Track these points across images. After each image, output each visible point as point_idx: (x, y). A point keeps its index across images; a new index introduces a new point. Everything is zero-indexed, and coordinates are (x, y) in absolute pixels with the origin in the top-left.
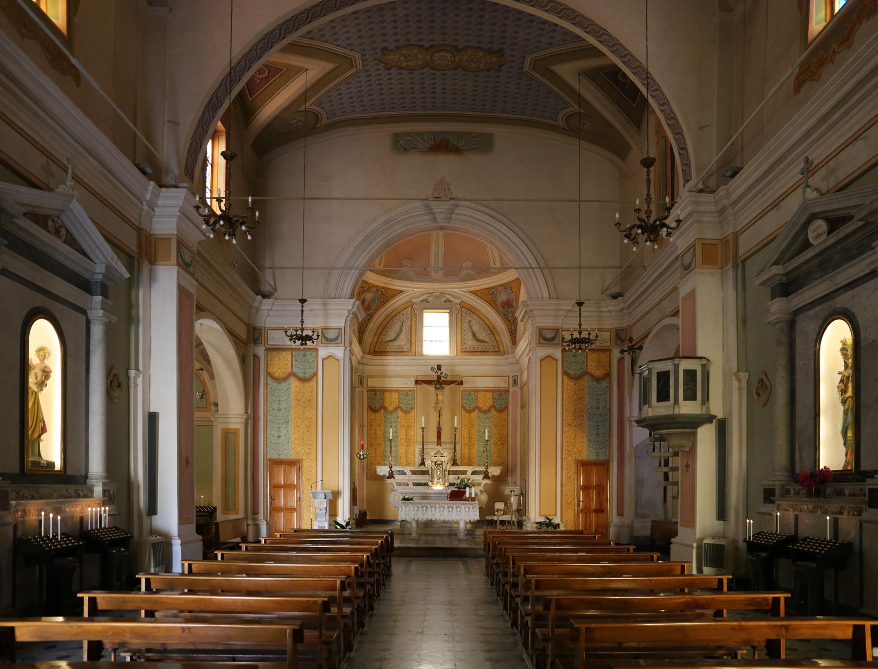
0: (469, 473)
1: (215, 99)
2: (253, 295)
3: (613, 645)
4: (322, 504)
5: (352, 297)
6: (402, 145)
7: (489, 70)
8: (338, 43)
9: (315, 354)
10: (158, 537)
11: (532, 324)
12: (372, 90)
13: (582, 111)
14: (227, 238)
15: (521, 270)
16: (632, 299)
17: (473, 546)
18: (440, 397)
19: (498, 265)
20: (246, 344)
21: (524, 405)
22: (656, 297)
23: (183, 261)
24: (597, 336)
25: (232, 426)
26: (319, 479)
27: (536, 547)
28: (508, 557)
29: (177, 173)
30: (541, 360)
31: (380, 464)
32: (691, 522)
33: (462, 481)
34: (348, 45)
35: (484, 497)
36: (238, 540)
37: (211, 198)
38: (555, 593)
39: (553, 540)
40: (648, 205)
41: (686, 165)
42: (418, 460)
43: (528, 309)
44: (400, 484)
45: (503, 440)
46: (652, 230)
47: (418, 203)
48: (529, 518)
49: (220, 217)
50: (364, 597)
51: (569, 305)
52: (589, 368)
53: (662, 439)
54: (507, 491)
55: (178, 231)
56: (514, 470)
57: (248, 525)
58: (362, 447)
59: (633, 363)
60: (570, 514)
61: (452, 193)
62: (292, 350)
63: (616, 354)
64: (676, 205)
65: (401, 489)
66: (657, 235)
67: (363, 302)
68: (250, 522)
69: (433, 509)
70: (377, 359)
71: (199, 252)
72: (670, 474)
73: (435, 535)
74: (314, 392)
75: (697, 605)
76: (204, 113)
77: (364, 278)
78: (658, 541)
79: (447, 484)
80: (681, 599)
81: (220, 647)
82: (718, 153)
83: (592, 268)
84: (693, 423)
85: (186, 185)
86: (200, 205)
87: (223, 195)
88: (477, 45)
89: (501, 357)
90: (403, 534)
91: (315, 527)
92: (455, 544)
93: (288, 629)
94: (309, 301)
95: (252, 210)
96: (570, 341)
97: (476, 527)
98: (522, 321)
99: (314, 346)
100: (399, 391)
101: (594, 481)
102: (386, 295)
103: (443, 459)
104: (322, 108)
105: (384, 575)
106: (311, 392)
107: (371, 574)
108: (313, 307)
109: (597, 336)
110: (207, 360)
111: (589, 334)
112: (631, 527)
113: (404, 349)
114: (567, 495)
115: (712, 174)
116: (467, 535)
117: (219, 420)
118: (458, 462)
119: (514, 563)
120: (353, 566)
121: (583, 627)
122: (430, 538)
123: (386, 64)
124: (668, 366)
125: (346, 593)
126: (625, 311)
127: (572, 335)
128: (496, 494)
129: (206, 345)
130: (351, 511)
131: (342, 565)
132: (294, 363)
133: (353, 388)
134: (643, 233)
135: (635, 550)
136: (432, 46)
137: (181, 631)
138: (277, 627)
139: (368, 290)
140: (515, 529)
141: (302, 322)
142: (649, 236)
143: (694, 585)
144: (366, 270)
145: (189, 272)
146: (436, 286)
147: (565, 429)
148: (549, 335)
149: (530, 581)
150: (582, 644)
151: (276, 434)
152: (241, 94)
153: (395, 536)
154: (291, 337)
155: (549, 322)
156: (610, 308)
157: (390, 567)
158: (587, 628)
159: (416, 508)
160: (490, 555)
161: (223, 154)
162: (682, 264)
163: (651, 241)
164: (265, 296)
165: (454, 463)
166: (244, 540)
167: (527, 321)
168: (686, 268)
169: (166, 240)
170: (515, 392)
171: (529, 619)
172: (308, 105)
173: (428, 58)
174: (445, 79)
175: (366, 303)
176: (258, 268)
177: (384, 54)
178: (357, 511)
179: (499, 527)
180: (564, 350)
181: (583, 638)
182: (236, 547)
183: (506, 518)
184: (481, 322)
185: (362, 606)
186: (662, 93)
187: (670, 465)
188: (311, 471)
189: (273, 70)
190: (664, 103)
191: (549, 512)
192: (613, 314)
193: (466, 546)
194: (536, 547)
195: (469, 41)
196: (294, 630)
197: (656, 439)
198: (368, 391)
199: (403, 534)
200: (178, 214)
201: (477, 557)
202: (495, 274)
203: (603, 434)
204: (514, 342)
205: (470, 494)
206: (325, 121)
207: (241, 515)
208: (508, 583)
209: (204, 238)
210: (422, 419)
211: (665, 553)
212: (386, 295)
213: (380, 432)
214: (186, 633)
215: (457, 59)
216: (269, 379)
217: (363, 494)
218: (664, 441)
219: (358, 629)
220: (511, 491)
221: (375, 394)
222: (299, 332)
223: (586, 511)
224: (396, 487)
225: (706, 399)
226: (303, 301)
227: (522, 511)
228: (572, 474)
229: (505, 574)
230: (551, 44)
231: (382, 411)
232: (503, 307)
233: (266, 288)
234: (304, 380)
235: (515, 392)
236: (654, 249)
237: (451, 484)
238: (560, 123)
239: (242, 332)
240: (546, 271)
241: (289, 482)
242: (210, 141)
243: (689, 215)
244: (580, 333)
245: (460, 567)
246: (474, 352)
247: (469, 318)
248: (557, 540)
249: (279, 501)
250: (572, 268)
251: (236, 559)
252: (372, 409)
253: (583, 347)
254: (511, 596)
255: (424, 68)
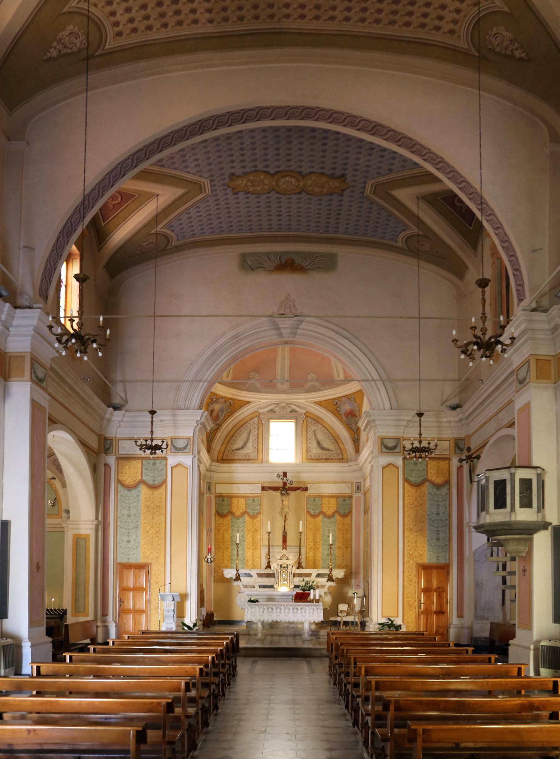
0: (313, 576)
1: (69, 225)
2: (103, 406)
3: (451, 745)
4: (170, 606)
5: (200, 408)
6: (249, 264)
7: (331, 194)
8: (188, 170)
9: (165, 461)
10: (9, 640)
11: (375, 433)
12: (221, 213)
13: (421, 233)
14: (78, 355)
15: (363, 383)
16: (469, 411)
17: (318, 646)
18: (285, 503)
19: (342, 377)
20: (97, 453)
21: (367, 511)
22: (493, 408)
23: (37, 377)
24: (436, 445)
25: (83, 532)
26: (168, 581)
27: (378, 648)
28: (350, 658)
29: (31, 294)
30: (383, 468)
31: (227, 567)
32: (528, 625)
33: (307, 583)
34: (197, 171)
35: (328, 599)
36: (88, 641)
37: (65, 317)
38: (397, 693)
39: (394, 642)
40: (484, 323)
41: (520, 285)
42: (264, 563)
43: (370, 419)
44: (246, 587)
45: (347, 544)
46: (488, 346)
47: (264, 320)
48: (371, 619)
49: (72, 336)
50: (209, 696)
51: (411, 415)
52: (429, 475)
53: (499, 544)
54: (350, 593)
55: (32, 349)
56: (357, 573)
57: (97, 627)
58: (210, 551)
59: (471, 471)
60: (412, 615)
61: (297, 310)
62: (142, 458)
63: (455, 462)
64: (511, 323)
65: (247, 591)
66: (493, 351)
67: (212, 412)
68: (99, 624)
69: (279, 610)
70: (225, 467)
71: (52, 368)
72: (508, 578)
73: (280, 635)
74: (163, 499)
75: (532, 707)
76: (58, 238)
77: (213, 390)
78: (496, 644)
79: (292, 586)
80: (518, 701)
81: (66, 747)
82: (551, 273)
83: (431, 380)
84: (529, 530)
85: (40, 305)
86: (53, 324)
87: (75, 314)
88: (321, 171)
89: (345, 465)
90: (249, 635)
91: (163, 629)
92: (299, 645)
93: (132, 731)
94: (159, 412)
95: (103, 328)
96: (410, 450)
97: (321, 628)
98: (364, 430)
99: (163, 455)
100: (246, 497)
101: (435, 584)
102: (233, 406)
103: (289, 562)
104: (173, 231)
105: (229, 675)
106: (160, 498)
107: (216, 674)
108: (161, 418)
109: (436, 445)
110: (59, 469)
111: (429, 443)
112: (471, 629)
113: (251, 457)
114: (408, 597)
115: (544, 295)
116: (311, 635)
117: (70, 526)
118: (303, 565)
119: (355, 664)
120: (198, 667)
121: (420, 727)
122: (275, 638)
123: (234, 189)
124: (504, 475)
125: (193, 693)
126: (463, 422)
127: (412, 444)
128: (340, 597)
129: (58, 455)
130: (199, 613)
131: (189, 667)
132: (144, 471)
133: (201, 495)
134: (479, 349)
135: (474, 652)
136: (277, 172)
137: (26, 733)
138: (121, 728)
139: (217, 401)
140: (358, 630)
141: (152, 432)
142: (484, 352)
143: (529, 688)
144: (214, 383)
145: (42, 388)
146: (282, 397)
147: (407, 534)
148: (391, 444)
149: (370, 682)
150: (419, 744)
151: (126, 539)
152: (94, 220)
153: (240, 637)
154: (141, 447)
155: (390, 432)
156: (449, 419)
157: (235, 667)
158: (423, 730)
159: (262, 610)
160: (333, 656)
161: (76, 277)
162: (517, 378)
163: (486, 357)
164: (116, 408)
165: (300, 566)
166: (94, 641)
167: (369, 431)
168: (521, 383)
169: (21, 357)
170: (358, 499)
171: (369, 719)
172: (159, 228)
173: (274, 183)
174: (290, 203)
175: (215, 414)
176: (110, 382)
177: (232, 180)
178: (204, 613)
179: (342, 627)
180: (405, 458)
181: (420, 739)
182: (84, 649)
183: (350, 619)
184: (326, 431)
185: (207, 705)
186: (497, 218)
187: (508, 569)
188: (159, 574)
189: (126, 197)
190: (498, 227)
191: (391, 613)
192: (452, 424)
193: (311, 646)
194: (378, 648)
195: (313, 167)
196: (137, 732)
197: (494, 545)
198: (216, 497)
199: (249, 635)
200: (33, 333)
201: (321, 657)
202: (338, 385)
203: (443, 539)
204: (357, 451)
205: (315, 596)
206: (174, 243)
207: (90, 617)
208: (349, 683)
209: (57, 355)
210: (268, 525)
211: (503, 652)
212: (233, 406)
213: (227, 536)
214: (32, 735)
215: (301, 184)
216: (120, 486)
217: (210, 596)
218: (502, 546)
219: (203, 728)
220: (354, 593)
221: (223, 500)
222: (149, 442)
223: (427, 612)
224: (243, 589)
225: (542, 506)
226: (153, 412)
227: (365, 612)
228: (413, 577)
229: (348, 674)
230: (390, 170)
231: (230, 517)
232: (347, 417)
233: (117, 401)
234: (153, 487)
235: (358, 499)
236: (490, 365)
237: (297, 587)
238: (400, 244)
239: (94, 443)
240: (387, 383)
241: (138, 585)
242: (65, 264)
243: (523, 333)
244: (420, 442)
245: (304, 666)
246: (318, 460)
247: (313, 428)
248: (398, 642)
249: (128, 604)
250: (413, 380)
251: (83, 661)
252: (220, 514)
253: (423, 456)
254: (353, 696)
255: (269, 193)
